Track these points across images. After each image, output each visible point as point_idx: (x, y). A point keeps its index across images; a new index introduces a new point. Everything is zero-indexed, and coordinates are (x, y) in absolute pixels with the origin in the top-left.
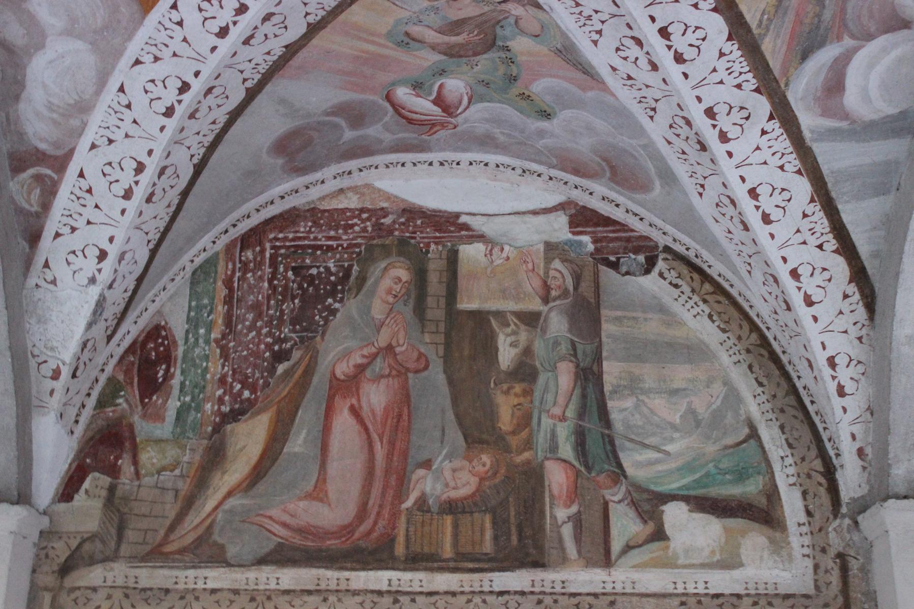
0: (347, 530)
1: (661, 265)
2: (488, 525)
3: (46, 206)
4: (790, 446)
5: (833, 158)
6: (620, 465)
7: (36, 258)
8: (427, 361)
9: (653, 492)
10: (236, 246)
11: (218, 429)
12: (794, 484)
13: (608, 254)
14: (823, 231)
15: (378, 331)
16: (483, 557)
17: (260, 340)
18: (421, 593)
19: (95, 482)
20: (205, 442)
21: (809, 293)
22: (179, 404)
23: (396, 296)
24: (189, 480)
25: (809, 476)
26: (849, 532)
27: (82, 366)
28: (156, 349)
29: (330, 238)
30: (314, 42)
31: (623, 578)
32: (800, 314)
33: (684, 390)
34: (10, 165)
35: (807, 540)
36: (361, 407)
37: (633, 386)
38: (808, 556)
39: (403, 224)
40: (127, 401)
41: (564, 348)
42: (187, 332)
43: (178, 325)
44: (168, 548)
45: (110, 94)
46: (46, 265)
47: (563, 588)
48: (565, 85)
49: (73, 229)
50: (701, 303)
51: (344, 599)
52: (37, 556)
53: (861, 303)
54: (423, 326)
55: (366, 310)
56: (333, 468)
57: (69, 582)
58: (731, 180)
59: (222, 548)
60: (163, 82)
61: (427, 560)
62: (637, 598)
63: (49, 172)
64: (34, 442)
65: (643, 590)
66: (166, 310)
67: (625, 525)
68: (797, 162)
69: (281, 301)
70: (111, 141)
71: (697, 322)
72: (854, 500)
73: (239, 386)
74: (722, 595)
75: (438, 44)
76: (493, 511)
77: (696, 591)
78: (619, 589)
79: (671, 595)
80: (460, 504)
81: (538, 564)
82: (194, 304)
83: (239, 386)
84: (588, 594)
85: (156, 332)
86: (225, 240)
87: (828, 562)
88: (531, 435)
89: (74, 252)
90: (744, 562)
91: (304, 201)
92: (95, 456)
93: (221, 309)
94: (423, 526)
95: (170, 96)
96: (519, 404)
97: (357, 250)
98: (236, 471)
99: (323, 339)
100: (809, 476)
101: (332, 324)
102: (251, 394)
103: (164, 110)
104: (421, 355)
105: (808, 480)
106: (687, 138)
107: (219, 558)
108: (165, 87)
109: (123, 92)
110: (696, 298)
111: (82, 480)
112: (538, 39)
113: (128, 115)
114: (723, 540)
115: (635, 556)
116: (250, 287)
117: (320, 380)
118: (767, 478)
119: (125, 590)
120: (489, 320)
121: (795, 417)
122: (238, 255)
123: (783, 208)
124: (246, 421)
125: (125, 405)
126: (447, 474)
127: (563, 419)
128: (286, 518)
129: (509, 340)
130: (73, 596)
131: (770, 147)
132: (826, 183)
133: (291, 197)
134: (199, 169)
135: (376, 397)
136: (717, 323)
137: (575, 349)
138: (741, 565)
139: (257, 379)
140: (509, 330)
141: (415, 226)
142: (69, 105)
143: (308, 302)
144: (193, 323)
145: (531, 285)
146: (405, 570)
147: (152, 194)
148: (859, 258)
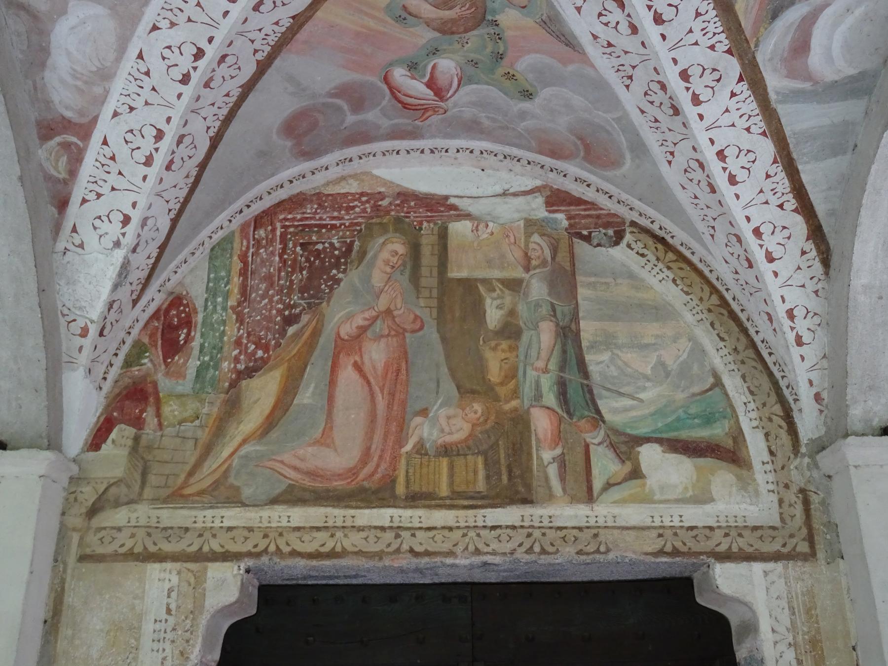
0: (353, 472)
1: (628, 237)
2: (481, 466)
3: (73, 173)
4: (752, 393)
5: (797, 119)
6: (598, 412)
7: (65, 224)
8: (422, 321)
9: (629, 435)
10: (249, 226)
11: (234, 384)
12: (757, 427)
13: (580, 229)
14: (785, 191)
15: (378, 297)
16: (477, 495)
17: (272, 307)
18: (420, 528)
19: (121, 433)
20: (223, 396)
21: (770, 250)
22: (199, 363)
23: (393, 267)
24: (207, 430)
25: (770, 420)
26: (809, 470)
27: (108, 326)
28: (178, 316)
29: (333, 218)
30: (319, 14)
31: (605, 512)
32: (762, 269)
33: (654, 344)
34: (38, 133)
35: (771, 477)
36: (363, 363)
37: (608, 342)
38: (773, 491)
39: (398, 205)
40: (151, 361)
41: (545, 310)
42: (206, 300)
43: (197, 293)
44: (187, 491)
45: (130, 62)
46: (74, 230)
47: (551, 522)
48: (547, 60)
49: (99, 196)
50: (665, 270)
51: (349, 535)
52: (67, 499)
53: (817, 259)
54: (418, 291)
55: (367, 279)
56: (339, 417)
57: (96, 522)
58: (701, 142)
59: (237, 489)
60: (179, 48)
61: (425, 499)
62: (619, 531)
63: (74, 139)
64: (64, 394)
65: (624, 524)
66: (187, 281)
67: (605, 465)
68: (762, 124)
69: (291, 272)
70: (132, 109)
71: (661, 284)
72: (811, 440)
73: (253, 347)
74: (696, 527)
75: (433, 20)
76: (484, 454)
77: (672, 524)
78: (601, 523)
79: (649, 528)
80: (454, 448)
81: (526, 501)
82: (212, 276)
83: (253, 347)
84: (574, 528)
85: (177, 301)
86: (239, 220)
87: (791, 496)
88: (517, 387)
89: (100, 217)
90: (715, 497)
91: (310, 186)
92: (121, 410)
93: (236, 280)
94: (421, 468)
95: (185, 63)
96: (506, 359)
97: (358, 228)
98: (252, 419)
99: (328, 305)
100: (770, 420)
101: (336, 292)
102: (264, 353)
103: (180, 77)
104: (416, 317)
105: (769, 423)
106: (661, 104)
107: (235, 500)
108: (181, 54)
109: (142, 59)
110: (660, 265)
111: (109, 431)
112: (525, 10)
113: (147, 83)
114: (695, 477)
115: (615, 494)
116: (263, 261)
117: (326, 341)
118: (732, 422)
119: (147, 529)
120: (477, 287)
121: (755, 368)
122: (251, 233)
123: (748, 169)
124: (260, 376)
125: (149, 365)
126: (443, 421)
127: (546, 371)
128: (297, 463)
129: (496, 303)
130: (100, 535)
131: (738, 109)
132: (788, 144)
133: (298, 182)
134: (215, 142)
135: (376, 354)
136: (680, 287)
137: (554, 310)
138: (712, 500)
139: (270, 340)
140: (495, 295)
141: (410, 207)
142: (91, 72)
143: (315, 273)
144: (212, 293)
145: (514, 255)
146: (405, 507)
147: (171, 162)
148: (816, 216)
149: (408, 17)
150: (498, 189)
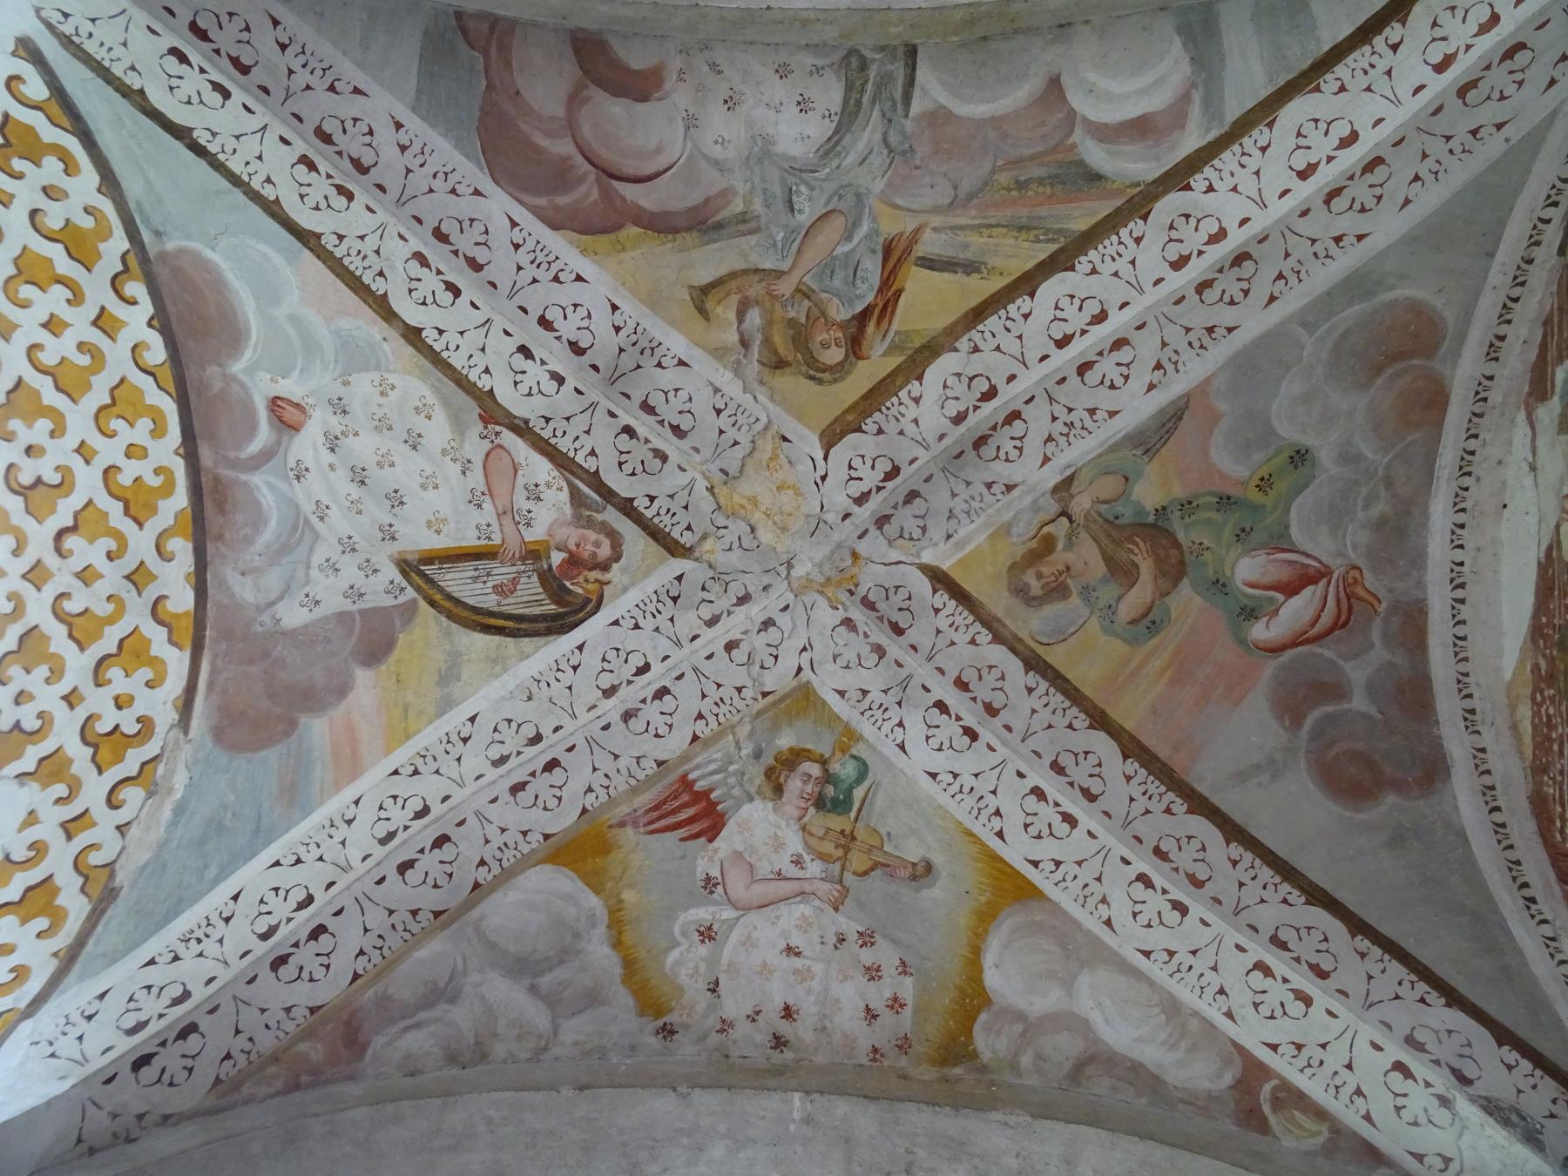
3: (1321, 1114)
45: (1155, 969)
112: (1131, 478)
149: (1151, 617)
150: (1528, 481)
